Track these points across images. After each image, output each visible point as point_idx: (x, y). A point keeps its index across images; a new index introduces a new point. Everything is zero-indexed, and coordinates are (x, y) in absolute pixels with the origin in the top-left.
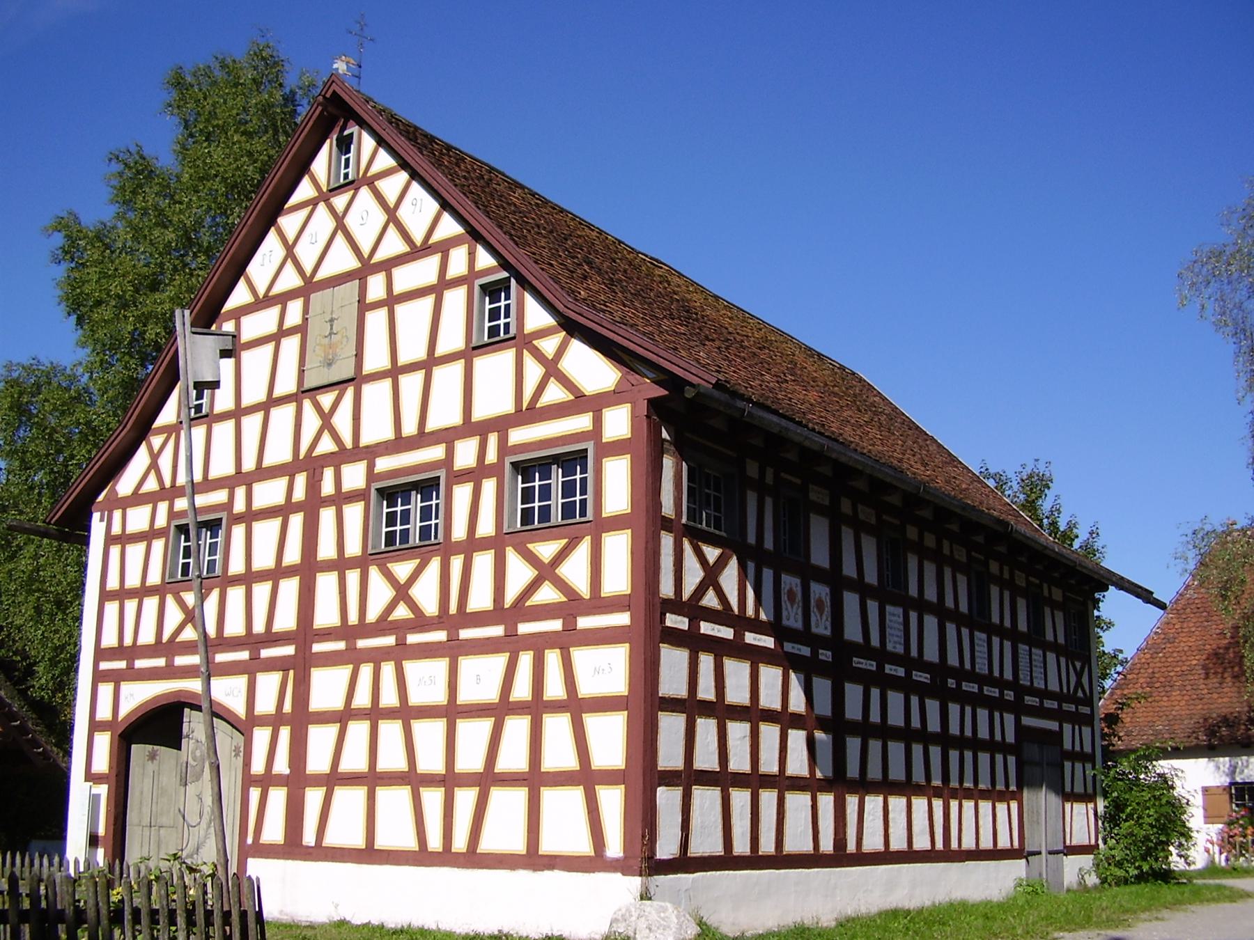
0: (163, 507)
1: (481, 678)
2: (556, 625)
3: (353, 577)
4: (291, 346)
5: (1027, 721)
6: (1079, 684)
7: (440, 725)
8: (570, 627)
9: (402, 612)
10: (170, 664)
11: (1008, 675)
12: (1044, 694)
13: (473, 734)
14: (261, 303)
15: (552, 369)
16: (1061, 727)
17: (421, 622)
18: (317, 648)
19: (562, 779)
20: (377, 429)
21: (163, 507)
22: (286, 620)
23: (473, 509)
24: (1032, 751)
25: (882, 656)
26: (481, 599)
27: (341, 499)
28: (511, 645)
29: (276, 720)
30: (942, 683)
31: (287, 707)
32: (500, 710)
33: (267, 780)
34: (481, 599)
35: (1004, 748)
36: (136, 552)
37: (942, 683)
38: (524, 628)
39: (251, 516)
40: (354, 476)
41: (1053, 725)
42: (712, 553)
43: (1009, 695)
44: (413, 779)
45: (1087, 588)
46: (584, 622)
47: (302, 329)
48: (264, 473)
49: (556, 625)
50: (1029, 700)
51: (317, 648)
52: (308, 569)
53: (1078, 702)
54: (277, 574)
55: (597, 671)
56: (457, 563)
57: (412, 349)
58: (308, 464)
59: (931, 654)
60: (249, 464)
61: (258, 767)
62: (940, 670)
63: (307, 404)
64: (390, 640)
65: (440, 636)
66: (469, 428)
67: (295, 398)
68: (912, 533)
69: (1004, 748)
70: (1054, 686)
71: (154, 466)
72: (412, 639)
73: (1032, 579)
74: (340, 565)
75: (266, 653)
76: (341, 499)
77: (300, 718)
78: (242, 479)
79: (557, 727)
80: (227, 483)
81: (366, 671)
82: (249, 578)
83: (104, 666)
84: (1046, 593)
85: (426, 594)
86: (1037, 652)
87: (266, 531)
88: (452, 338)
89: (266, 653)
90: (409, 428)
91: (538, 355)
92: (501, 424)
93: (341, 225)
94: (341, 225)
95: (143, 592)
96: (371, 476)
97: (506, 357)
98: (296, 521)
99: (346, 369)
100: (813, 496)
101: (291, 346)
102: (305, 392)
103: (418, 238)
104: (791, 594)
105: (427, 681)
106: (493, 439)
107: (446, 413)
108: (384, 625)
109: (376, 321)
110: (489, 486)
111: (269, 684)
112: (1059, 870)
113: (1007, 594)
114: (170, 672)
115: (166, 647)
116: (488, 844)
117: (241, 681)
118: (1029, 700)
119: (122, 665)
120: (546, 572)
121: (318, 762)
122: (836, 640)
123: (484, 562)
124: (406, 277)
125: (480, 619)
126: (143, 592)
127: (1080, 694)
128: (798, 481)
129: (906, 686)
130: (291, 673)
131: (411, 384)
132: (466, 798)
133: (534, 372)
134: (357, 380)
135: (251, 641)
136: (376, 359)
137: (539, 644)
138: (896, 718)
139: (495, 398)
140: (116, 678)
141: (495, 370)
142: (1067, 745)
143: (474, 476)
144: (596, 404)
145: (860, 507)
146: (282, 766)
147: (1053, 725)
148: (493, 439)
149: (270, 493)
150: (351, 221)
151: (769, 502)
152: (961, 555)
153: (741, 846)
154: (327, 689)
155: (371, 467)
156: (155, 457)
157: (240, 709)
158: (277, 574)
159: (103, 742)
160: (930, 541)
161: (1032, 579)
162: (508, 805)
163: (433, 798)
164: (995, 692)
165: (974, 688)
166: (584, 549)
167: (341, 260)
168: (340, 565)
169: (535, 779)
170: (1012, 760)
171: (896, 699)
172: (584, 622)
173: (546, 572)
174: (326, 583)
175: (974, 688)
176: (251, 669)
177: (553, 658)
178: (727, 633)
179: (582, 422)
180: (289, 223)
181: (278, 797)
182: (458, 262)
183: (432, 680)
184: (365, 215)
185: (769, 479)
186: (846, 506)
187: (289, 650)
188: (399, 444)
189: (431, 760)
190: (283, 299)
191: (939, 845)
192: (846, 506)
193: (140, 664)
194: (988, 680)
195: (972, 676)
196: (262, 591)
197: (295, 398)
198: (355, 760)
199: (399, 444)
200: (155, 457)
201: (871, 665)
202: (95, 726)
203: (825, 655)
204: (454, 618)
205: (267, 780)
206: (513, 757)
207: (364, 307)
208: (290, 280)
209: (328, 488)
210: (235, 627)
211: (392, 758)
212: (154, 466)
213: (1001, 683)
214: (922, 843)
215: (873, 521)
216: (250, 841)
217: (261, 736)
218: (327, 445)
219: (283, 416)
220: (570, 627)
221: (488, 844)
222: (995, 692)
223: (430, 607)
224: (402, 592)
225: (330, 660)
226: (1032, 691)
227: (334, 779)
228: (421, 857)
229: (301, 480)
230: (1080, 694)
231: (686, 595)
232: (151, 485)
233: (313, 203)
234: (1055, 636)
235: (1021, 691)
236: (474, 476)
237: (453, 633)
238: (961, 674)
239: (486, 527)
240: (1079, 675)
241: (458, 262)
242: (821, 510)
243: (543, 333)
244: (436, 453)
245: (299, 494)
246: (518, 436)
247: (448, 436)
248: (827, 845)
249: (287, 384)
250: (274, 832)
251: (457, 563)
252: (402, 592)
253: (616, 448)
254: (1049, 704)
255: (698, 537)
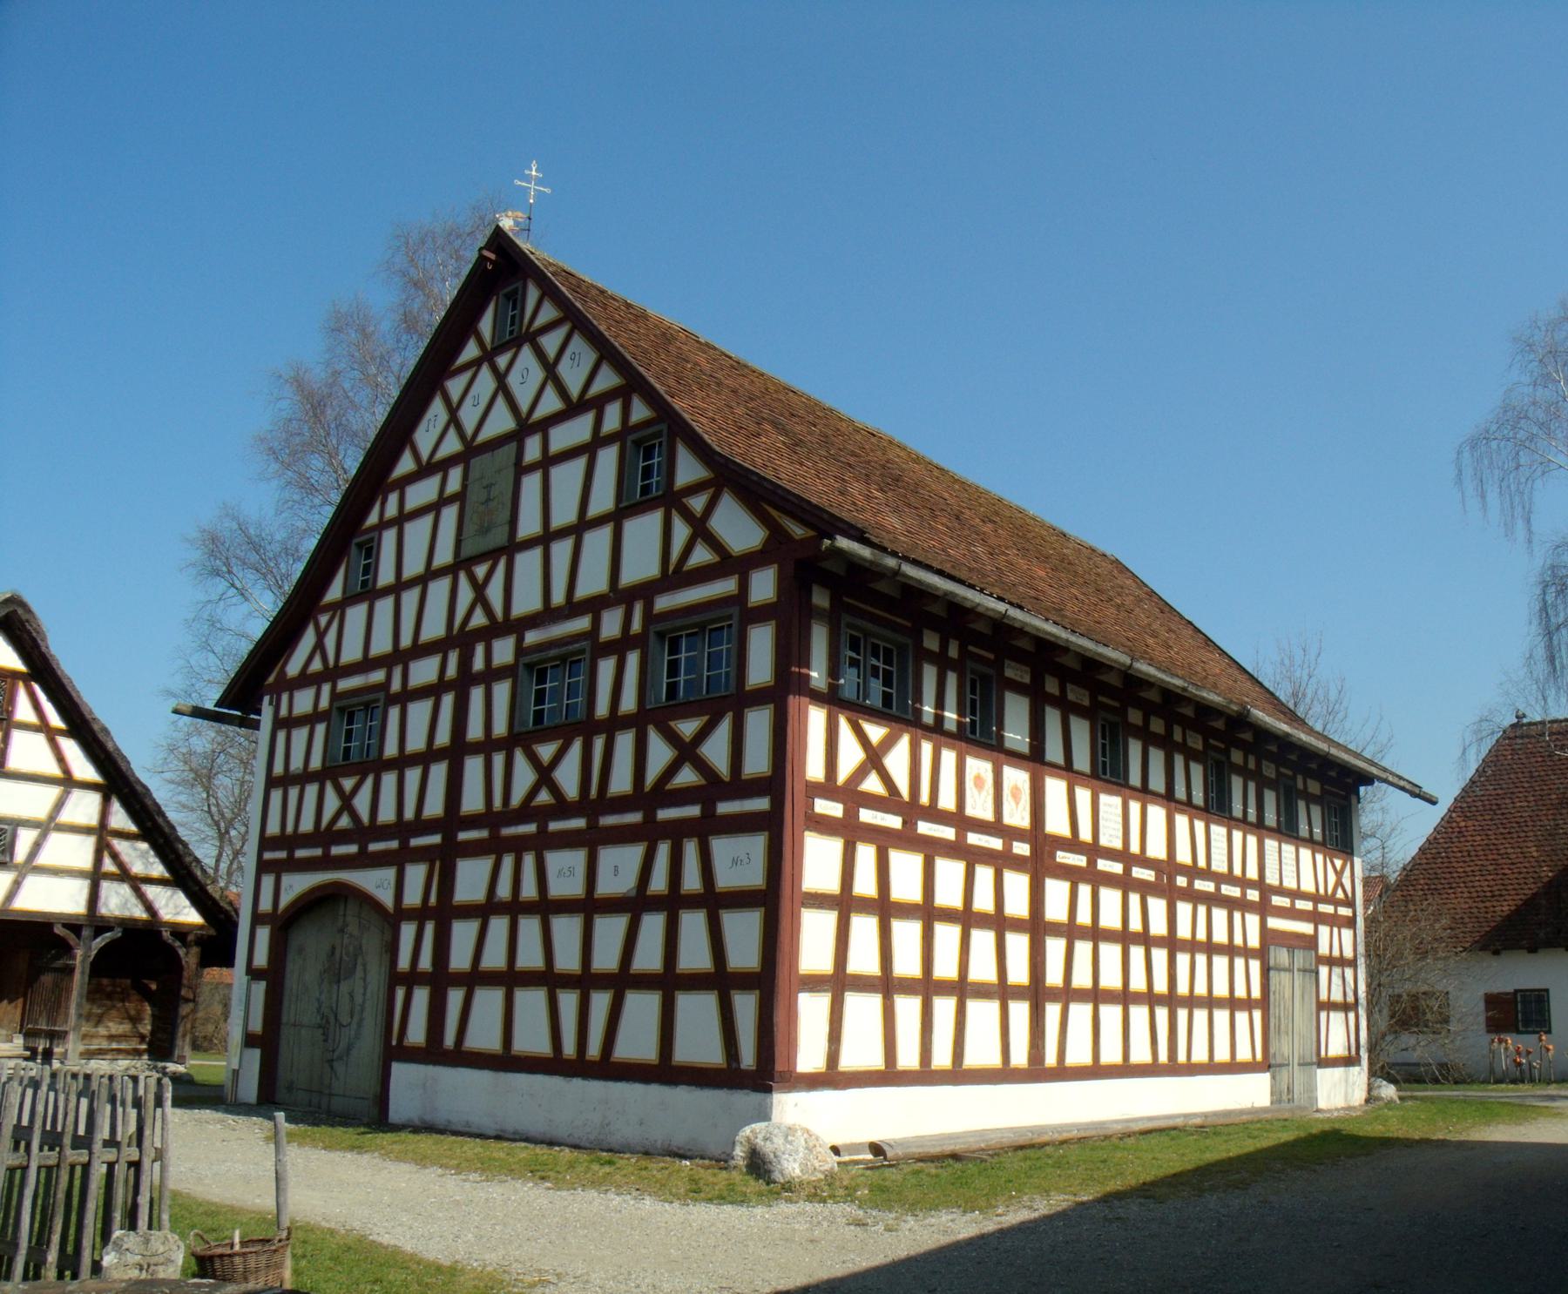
0: (326, 689)
1: (619, 868)
2: (694, 811)
3: (499, 760)
4: (450, 514)
5: (1274, 923)
6: (1339, 883)
7: (829, 919)
8: (709, 811)
9: (544, 797)
10: (326, 854)
11: (1252, 874)
12: (1296, 894)
13: (611, 929)
14: (424, 470)
15: (701, 531)
16: (1316, 930)
17: (562, 808)
18: (463, 836)
19: (696, 982)
20: (527, 601)
21: (326, 689)
22: (435, 806)
23: (617, 684)
24: (1280, 956)
25: (1094, 850)
26: (621, 782)
27: (491, 675)
28: (648, 834)
29: (420, 915)
30: (1171, 882)
31: (433, 900)
32: (635, 905)
33: (412, 979)
34: (621, 782)
35: (1247, 953)
36: (300, 736)
37: (1171, 882)
38: (664, 814)
39: (407, 696)
40: (504, 651)
41: (1306, 928)
42: (876, 732)
43: (1253, 895)
44: (549, 979)
45: (1349, 780)
46: (724, 808)
47: (460, 497)
48: (421, 650)
49: (694, 811)
50: (1277, 901)
51: (463, 836)
52: (457, 751)
53: (1337, 903)
54: (425, 759)
55: (735, 862)
56: (599, 744)
57: (564, 514)
58: (460, 640)
59: (1157, 850)
60: (406, 641)
61: (404, 963)
62: (1169, 867)
63: (463, 577)
64: (531, 828)
65: (579, 823)
66: (619, 595)
67: (451, 570)
68: (1135, 717)
69: (1247, 953)
70: (1308, 886)
71: (319, 646)
72: (554, 826)
73: (1283, 770)
74: (487, 746)
75: (415, 842)
76: (491, 675)
77: (442, 912)
78: (400, 657)
79: (693, 924)
80: (386, 662)
81: (508, 861)
82: (402, 762)
83: (268, 855)
84: (1300, 785)
85: (568, 777)
86: (1289, 849)
87: (419, 712)
88: (603, 499)
89: (415, 842)
90: (558, 597)
91: (688, 515)
92: (646, 591)
93: (502, 388)
94: (502, 388)
95: (305, 778)
96: (520, 650)
97: (654, 519)
98: (448, 701)
99: (499, 537)
100: (1009, 673)
101: (450, 514)
102: (462, 564)
103: (575, 391)
104: (979, 781)
105: (565, 872)
106: (638, 609)
107: (593, 581)
108: (526, 812)
109: (531, 484)
110: (633, 659)
111: (416, 875)
112: (1311, 1088)
113: (1252, 786)
114: (327, 863)
115: (325, 836)
116: (622, 1052)
117: (389, 874)
118: (1277, 901)
119: (282, 855)
120: (687, 752)
121: (460, 960)
122: (1036, 832)
123: (625, 743)
124: (568, 435)
125: (622, 804)
126: (305, 778)
127: (1340, 894)
128: (991, 656)
129: (1125, 884)
130: (438, 864)
131: (561, 551)
132: (601, 1001)
133: (681, 532)
134: (512, 548)
135: (402, 829)
136: (529, 525)
137: (677, 832)
138: (1110, 919)
139: (641, 564)
140: (277, 868)
141: (643, 533)
142: (1323, 949)
143: (618, 648)
144: (740, 566)
145: (1069, 687)
146: (425, 963)
147: (1306, 928)
148: (638, 609)
149: (424, 671)
150: (513, 380)
151: (952, 680)
152: (1196, 742)
153: (908, 1058)
154: (471, 880)
155: (520, 640)
156: (321, 635)
157: (387, 898)
158: (425, 759)
159: (263, 934)
160: (1157, 726)
161: (1283, 770)
162: (642, 1008)
163: (568, 1001)
164: (1235, 892)
165: (1209, 886)
166: (724, 730)
167: (501, 422)
168: (487, 746)
169: (670, 982)
170: (1255, 965)
171: (1111, 898)
172: (724, 808)
173: (687, 752)
174: (473, 767)
175: (1209, 886)
176: (398, 860)
177: (691, 849)
178: (895, 822)
179: (727, 586)
180: (455, 386)
181: (421, 996)
182: (612, 419)
183: (571, 871)
184: (525, 374)
185: (953, 652)
186: (1052, 686)
187: (436, 839)
188: (548, 615)
189: (568, 960)
190: (444, 466)
191: (1163, 1057)
192: (1052, 686)
193: (301, 853)
194: (1229, 878)
195: (1207, 874)
196: (413, 776)
197: (451, 570)
198: (494, 958)
199: (548, 615)
200: (321, 635)
201: (1080, 861)
202: (257, 919)
203: (1022, 849)
204: (594, 803)
205: (412, 979)
206: (649, 958)
207: (521, 470)
208: (452, 445)
209: (478, 664)
210: (387, 814)
211: (530, 957)
212: (319, 646)
213: (1244, 883)
214: (1141, 1054)
215: (1086, 702)
216: (394, 1043)
217: (408, 931)
218: (479, 619)
219: (439, 590)
220: (709, 811)
221: (622, 1052)
222: (1235, 892)
223: (571, 790)
224: (545, 775)
225: (474, 850)
226: (1281, 891)
227: (475, 978)
228: (553, 1065)
229: (453, 658)
230: (1340, 894)
231: (843, 775)
232: (317, 665)
233: (476, 364)
234: (1311, 831)
235: (1266, 890)
236: (618, 648)
237: (595, 820)
238: (1193, 872)
239: (629, 703)
240: (1339, 874)
241: (612, 419)
242: (1018, 688)
243: (694, 489)
244: (582, 624)
245: (452, 671)
246: (663, 603)
247: (595, 606)
248: (1020, 1058)
249: (444, 556)
250: (417, 1034)
251: (599, 744)
252: (545, 775)
253: (761, 614)
254: (1303, 905)
255: (858, 709)
